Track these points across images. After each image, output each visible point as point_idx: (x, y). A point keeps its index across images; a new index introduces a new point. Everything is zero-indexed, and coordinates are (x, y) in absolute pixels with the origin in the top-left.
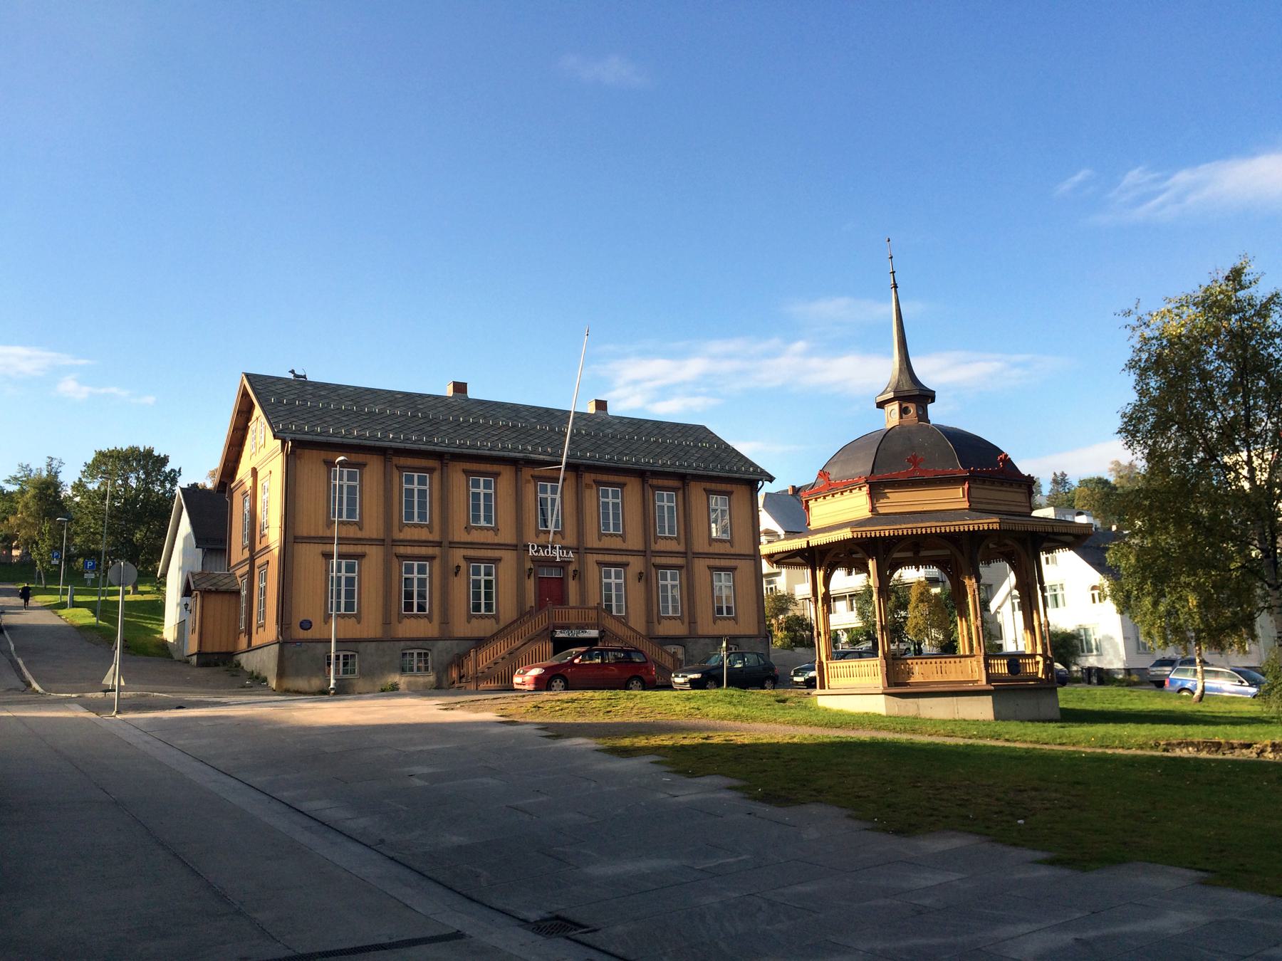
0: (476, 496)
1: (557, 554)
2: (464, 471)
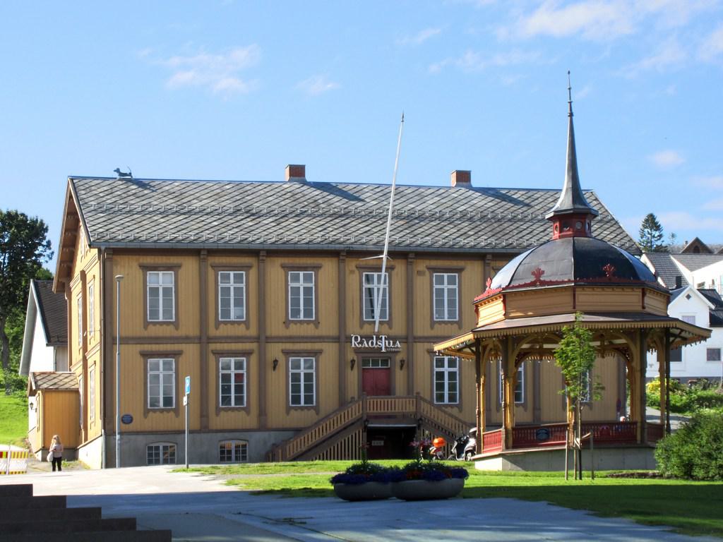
0: (440, 292)
1: (383, 344)
2: (283, 267)
